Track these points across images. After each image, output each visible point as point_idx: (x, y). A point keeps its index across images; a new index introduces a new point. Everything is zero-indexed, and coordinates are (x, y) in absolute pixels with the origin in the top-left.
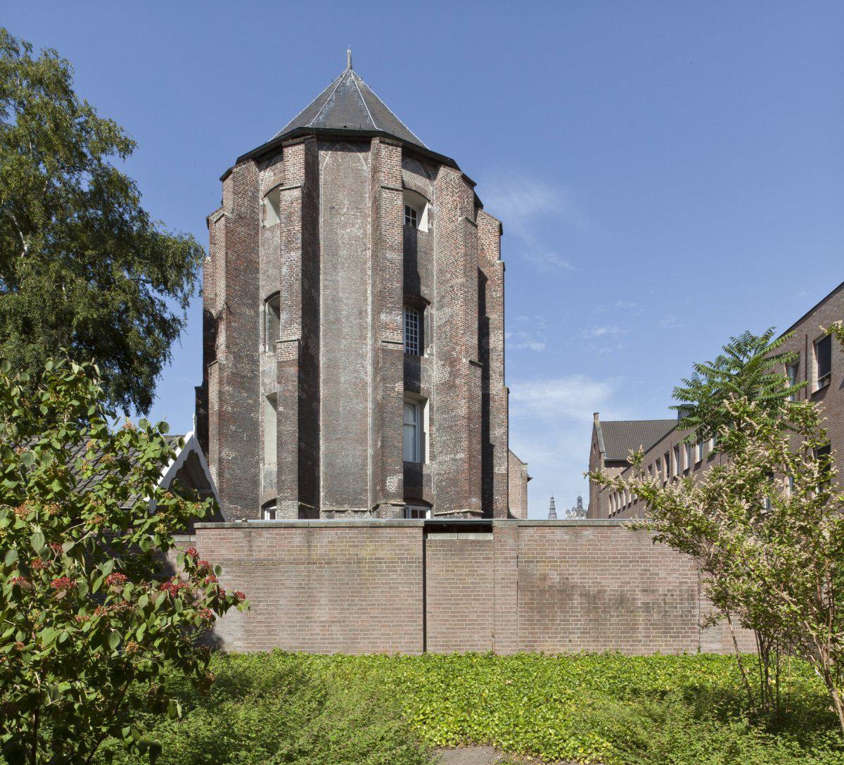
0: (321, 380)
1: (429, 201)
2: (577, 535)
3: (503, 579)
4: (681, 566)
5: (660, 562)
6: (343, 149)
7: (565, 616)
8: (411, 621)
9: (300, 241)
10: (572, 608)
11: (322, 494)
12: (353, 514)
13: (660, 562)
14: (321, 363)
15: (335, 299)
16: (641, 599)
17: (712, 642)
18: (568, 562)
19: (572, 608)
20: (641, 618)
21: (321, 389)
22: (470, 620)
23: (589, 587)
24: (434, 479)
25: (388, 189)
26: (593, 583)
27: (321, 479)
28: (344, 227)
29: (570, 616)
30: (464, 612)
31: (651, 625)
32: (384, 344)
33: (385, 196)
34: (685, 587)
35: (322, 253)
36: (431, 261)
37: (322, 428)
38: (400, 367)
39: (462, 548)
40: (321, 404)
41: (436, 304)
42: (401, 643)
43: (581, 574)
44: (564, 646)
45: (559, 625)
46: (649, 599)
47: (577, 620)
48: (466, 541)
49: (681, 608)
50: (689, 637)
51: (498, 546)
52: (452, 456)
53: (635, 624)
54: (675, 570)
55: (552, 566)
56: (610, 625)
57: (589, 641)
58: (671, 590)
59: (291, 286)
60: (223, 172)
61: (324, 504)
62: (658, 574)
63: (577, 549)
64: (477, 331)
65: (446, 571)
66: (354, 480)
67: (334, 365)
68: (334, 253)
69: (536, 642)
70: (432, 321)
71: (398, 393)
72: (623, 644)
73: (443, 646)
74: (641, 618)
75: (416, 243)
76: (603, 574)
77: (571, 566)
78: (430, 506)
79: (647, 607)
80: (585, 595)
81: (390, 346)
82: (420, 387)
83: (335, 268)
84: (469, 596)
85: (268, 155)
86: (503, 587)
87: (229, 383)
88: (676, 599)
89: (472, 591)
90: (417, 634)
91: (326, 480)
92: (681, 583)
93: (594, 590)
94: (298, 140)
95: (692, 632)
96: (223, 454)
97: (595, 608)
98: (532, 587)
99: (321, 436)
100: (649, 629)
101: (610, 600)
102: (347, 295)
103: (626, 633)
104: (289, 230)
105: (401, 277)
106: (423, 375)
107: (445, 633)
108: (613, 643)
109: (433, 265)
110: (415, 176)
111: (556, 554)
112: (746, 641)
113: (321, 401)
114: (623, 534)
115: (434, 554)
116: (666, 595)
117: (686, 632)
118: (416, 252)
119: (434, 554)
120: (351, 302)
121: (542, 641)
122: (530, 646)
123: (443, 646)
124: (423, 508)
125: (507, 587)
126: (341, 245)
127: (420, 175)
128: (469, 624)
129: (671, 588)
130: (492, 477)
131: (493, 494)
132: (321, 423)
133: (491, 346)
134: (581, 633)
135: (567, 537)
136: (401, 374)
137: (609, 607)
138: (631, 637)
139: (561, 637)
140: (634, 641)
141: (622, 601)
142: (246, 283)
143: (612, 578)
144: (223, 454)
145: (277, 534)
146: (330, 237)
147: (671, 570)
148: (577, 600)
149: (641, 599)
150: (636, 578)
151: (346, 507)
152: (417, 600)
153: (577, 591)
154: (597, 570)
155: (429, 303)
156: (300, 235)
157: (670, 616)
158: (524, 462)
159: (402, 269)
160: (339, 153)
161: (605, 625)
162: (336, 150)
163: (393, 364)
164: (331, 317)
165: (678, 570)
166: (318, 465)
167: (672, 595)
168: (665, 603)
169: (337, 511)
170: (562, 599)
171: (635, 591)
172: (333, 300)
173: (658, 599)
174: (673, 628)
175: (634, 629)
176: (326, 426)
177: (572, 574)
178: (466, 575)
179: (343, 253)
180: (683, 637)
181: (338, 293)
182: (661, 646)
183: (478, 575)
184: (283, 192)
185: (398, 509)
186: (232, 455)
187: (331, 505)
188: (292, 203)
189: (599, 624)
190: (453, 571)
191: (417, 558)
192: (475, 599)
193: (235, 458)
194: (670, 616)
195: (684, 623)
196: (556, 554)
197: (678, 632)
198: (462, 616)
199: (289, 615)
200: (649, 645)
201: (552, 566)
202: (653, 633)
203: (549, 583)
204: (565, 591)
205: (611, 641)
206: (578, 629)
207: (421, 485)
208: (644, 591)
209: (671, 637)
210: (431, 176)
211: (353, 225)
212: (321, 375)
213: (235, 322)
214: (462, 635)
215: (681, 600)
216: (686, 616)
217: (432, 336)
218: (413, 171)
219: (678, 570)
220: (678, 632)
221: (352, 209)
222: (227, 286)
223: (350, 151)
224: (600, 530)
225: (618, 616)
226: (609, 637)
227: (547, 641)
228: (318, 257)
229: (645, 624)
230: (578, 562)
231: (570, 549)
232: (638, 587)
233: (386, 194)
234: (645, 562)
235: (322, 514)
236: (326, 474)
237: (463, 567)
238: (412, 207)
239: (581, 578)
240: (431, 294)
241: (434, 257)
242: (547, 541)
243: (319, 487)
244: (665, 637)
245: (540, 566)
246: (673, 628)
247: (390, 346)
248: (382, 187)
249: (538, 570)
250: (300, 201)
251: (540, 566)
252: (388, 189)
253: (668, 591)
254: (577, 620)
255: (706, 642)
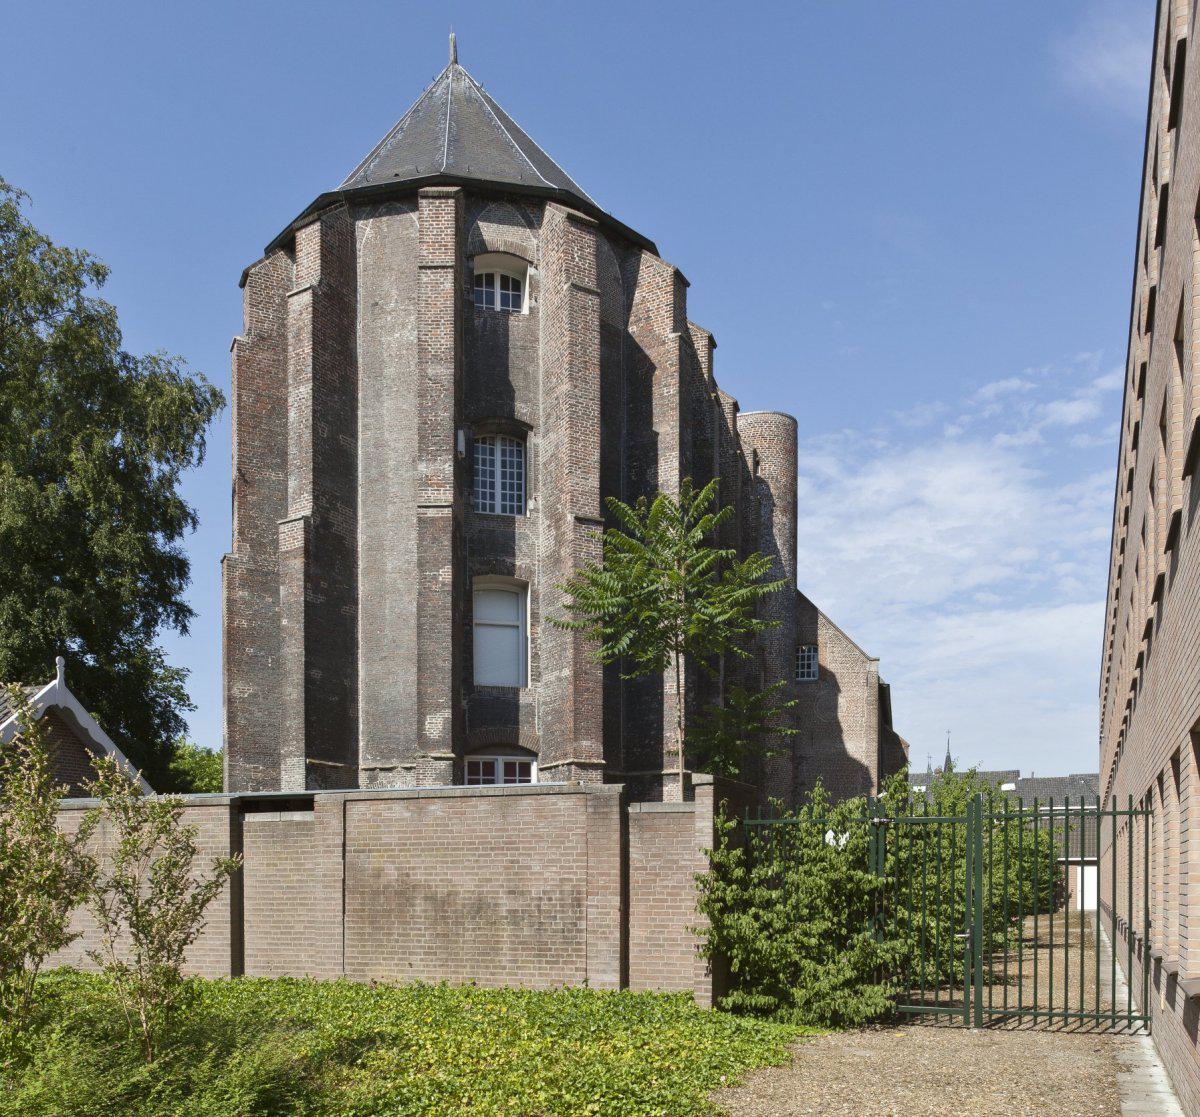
0: (360, 571)
1: (531, 263)
2: (421, 811)
3: (325, 876)
4: (562, 855)
5: (534, 849)
6: (389, 213)
7: (404, 929)
8: (216, 934)
9: (310, 369)
10: (413, 917)
11: (361, 744)
12: (404, 772)
13: (534, 849)
14: (360, 544)
15: (379, 445)
16: (506, 904)
17: (604, 971)
18: (409, 850)
19: (413, 917)
20: (506, 933)
21: (360, 585)
22: (296, 933)
23: (436, 886)
24: (540, 711)
25: (430, 268)
26: (441, 880)
27: (361, 720)
28: (392, 330)
29: (411, 929)
30: (288, 922)
31: (520, 943)
32: (421, 510)
33: (425, 279)
34: (567, 888)
35: (360, 376)
36: (533, 360)
37: (361, 643)
38: (446, 543)
39: (287, 832)
40: (360, 606)
41: (542, 429)
42: (205, 962)
43: (425, 869)
44: (402, 971)
45: (397, 941)
46: (518, 904)
47: (420, 935)
48: (290, 823)
49: (562, 918)
50: (572, 962)
51: (318, 829)
52: (556, 673)
53: (497, 942)
54: (553, 861)
55: (388, 857)
56: (464, 942)
57: (435, 966)
58: (548, 892)
59: (300, 436)
60: (239, 278)
61: (365, 759)
62: (530, 867)
63: (420, 832)
64: (597, 465)
65: (268, 865)
66: (405, 719)
67: (377, 546)
68: (378, 375)
69: (366, 964)
70: (536, 456)
71: (444, 584)
72: (480, 971)
73: (263, 967)
74: (506, 933)
75: (506, 336)
76: (455, 868)
77: (412, 856)
78: (535, 755)
79: (514, 917)
80: (431, 898)
81: (431, 513)
82: (514, 565)
83: (378, 396)
84: (295, 899)
85: (286, 243)
86: (326, 887)
87: (243, 586)
88: (555, 906)
89: (299, 893)
90: (223, 950)
91: (367, 723)
92: (561, 880)
93: (442, 891)
94: (311, 218)
95: (577, 956)
96: (235, 691)
97: (443, 917)
98: (363, 886)
99: (360, 655)
100: (516, 949)
101: (464, 905)
102: (395, 436)
103: (484, 954)
104: (298, 354)
105: (450, 402)
106: (521, 546)
107: (266, 950)
108: (468, 969)
109: (538, 365)
110: (505, 228)
111: (394, 839)
112: (670, 972)
113: (360, 601)
114: (482, 808)
115: (253, 842)
116: (540, 899)
117: (569, 955)
118: (507, 349)
119: (253, 842)
120: (401, 445)
121: (375, 964)
122: (359, 970)
123: (263, 967)
124: (525, 759)
125: (330, 887)
126: (387, 359)
127: (513, 224)
128: (295, 939)
129: (548, 888)
130: (662, 699)
131: (662, 730)
132: (360, 636)
133: (661, 480)
134: (426, 953)
135: (407, 815)
136: (447, 553)
137: (462, 917)
138: (492, 961)
139: (401, 959)
140: (495, 967)
141: (480, 907)
142: (271, 434)
143: (467, 874)
144: (235, 691)
145: (70, 818)
146: (371, 349)
147: (549, 861)
148: (420, 906)
149: (506, 904)
150: (501, 874)
151: (394, 762)
152: (223, 905)
153: (420, 893)
154: (447, 863)
155: (531, 428)
156: (310, 361)
157: (546, 930)
158: (872, 656)
159: (452, 389)
160: (384, 219)
161: (456, 942)
162: (380, 216)
163: (435, 540)
164: (374, 473)
165: (559, 861)
166: (355, 701)
167: (550, 899)
168: (539, 911)
169: (382, 769)
170: (400, 905)
171: (498, 893)
172: (376, 446)
173: (529, 905)
174: (550, 950)
175: (496, 950)
176: (368, 640)
177: (414, 868)
178: (291, 870)
179: (390, 371)
180: (565, 962)
181: (382, 434)
182: (533, 975)
183: (305, 870)
184: (291, 299)
185: (443, 764)
186: (250, 690)
187: (374, 760)
188: (301, 314)
189: (449, 942)
190: (276, 865)
191: (223, 848)
192: (301, 904)
193: (255, 695)
194: (546, 930)
195: (566, 941)
196: (394, 839)
197: (558, 956)
198: (286, 927)
199: (84, 923)
200: (516, 975)
201: (388, 857)
202: (523, 956)
203: (383, 881)
204: (405, 893)
205: (465, 967)
206: (421, 947)
207: (516, 722)
208: (510, 892)
209: (547, 962)
210: (533, 223)
211: (404, 326)
212: (360, 563)
213: (253, 494)
214: (285, 953)
215: (562, 906)
216: (570, 931)
217: (536, 480)
218: (500, 222)
219: (559, 861)
220: (558, 956)
221: (403, 302)
222: (239, 444)
223: (399, 212)
224: (451, 802)
225: (474, 930)
226: (462, 960)
227: (380, 964)
228: (355, 383)
229: (512, 942)
230: (422, 850)
231: (412, 832)
232: (502, 886)
233: (427, 277)
234: (512, 849)
235: (363, 778)
236: (367, 713)
237: (286, 859)
238: (511, 275)
239: (426, 874)
240: (534, 413)
241: (540, 353)
242: (383, 821)
243: (357, 732)
244: (540, 962)
245: (374, 857)
246: (550, 950)
247: (431, 513)
248: (421, 268)
249: (372, 862)
250: (310, 309)
251: (374, 857)
252: (430, 268)
253: (544, 892)
254: (420, 935)
255: (598, 971)
